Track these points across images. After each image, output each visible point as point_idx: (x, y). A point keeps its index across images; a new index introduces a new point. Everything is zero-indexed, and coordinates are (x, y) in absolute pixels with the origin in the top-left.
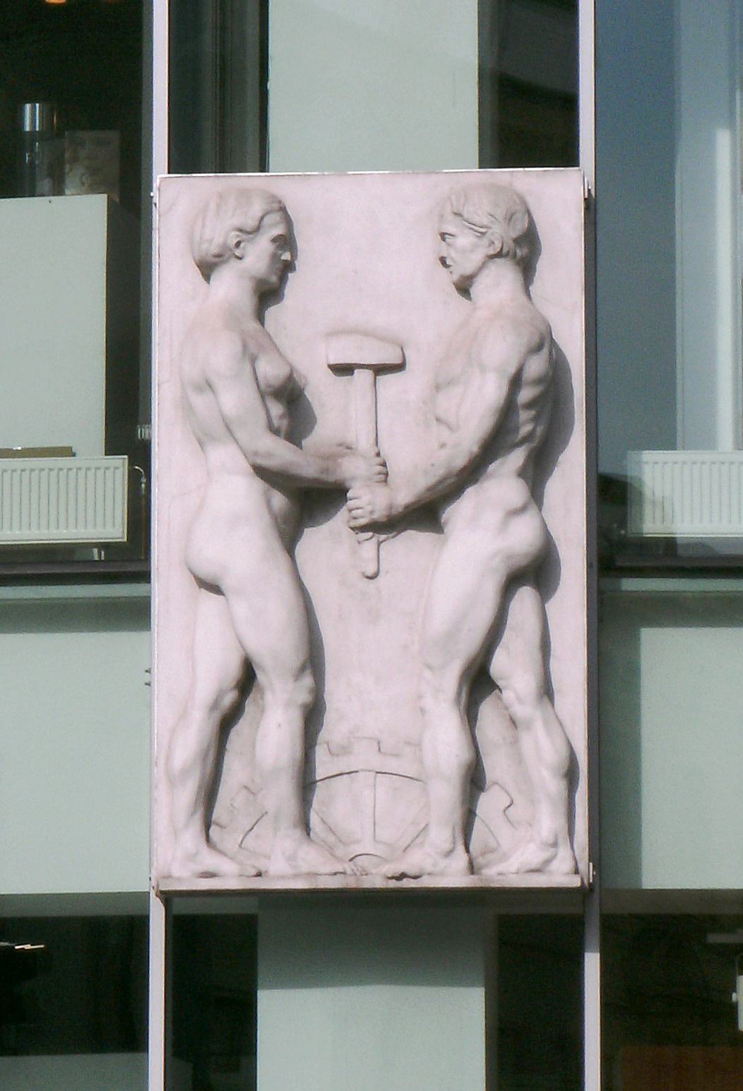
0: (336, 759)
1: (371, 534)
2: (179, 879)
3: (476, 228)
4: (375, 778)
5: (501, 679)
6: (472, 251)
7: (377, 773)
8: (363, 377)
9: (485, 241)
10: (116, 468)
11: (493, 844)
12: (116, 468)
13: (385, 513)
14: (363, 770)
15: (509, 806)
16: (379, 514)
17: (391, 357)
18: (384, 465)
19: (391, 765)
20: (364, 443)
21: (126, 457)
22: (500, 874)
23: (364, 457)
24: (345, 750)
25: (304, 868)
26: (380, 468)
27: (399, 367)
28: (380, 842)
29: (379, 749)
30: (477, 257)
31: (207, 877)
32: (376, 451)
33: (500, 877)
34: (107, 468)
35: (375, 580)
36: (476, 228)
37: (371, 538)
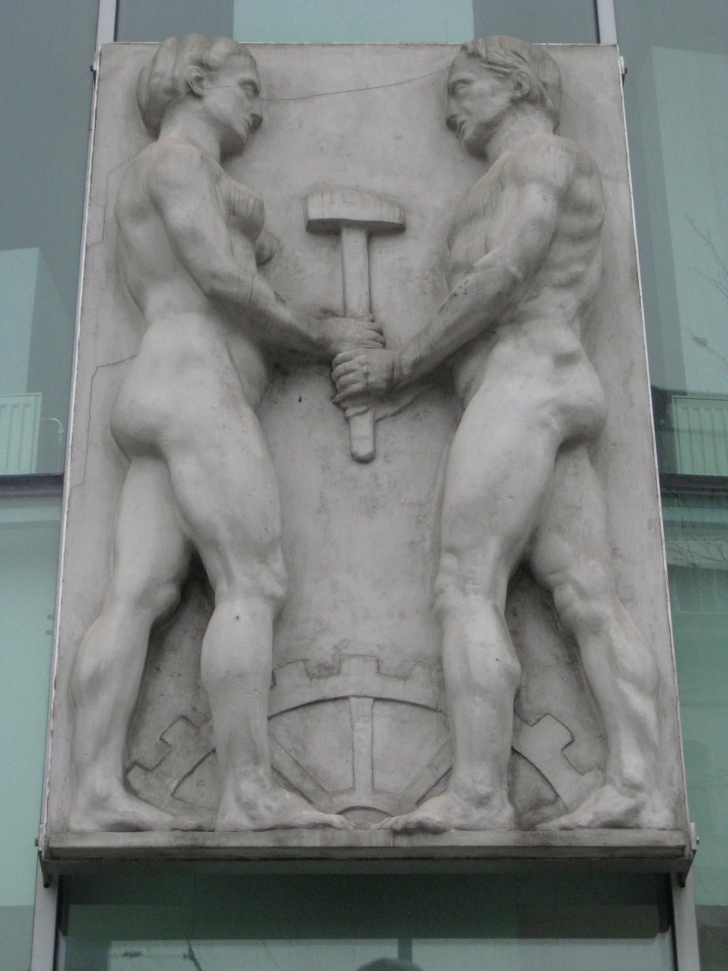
0: (315, 681)
1: (364, 408)
2: (82, 834)
3: (498, 68)
4: (373, 705)
5: (552, 573)
6: (493, 95)
7: (377, 699)
8: (353, 241)
9: (511, 84)
10: (27, 406)
11: (549, 795)
12: (27, 406)
13: (384, 375)
14: (354, 696)
15: (569, 744)
16: (378, 378)
17: (388, 215)
18: (380, 332)
19: (395, 690)
20: (356, 302)
21: (40, 393)
22: (564, 828)
23: (355, 317)
24: (329, 670)
25: (269, 820)
26: (375, 334)
27: (396, 230)
28: (382, 792)
29: (378, 669)
30: (501, 100)
31: (116, 555)
32: (371, 317)
33: (565, 833)
34: (16, 406)
35: (370, 464)
36: (498, 68)
37: (365, 412)
